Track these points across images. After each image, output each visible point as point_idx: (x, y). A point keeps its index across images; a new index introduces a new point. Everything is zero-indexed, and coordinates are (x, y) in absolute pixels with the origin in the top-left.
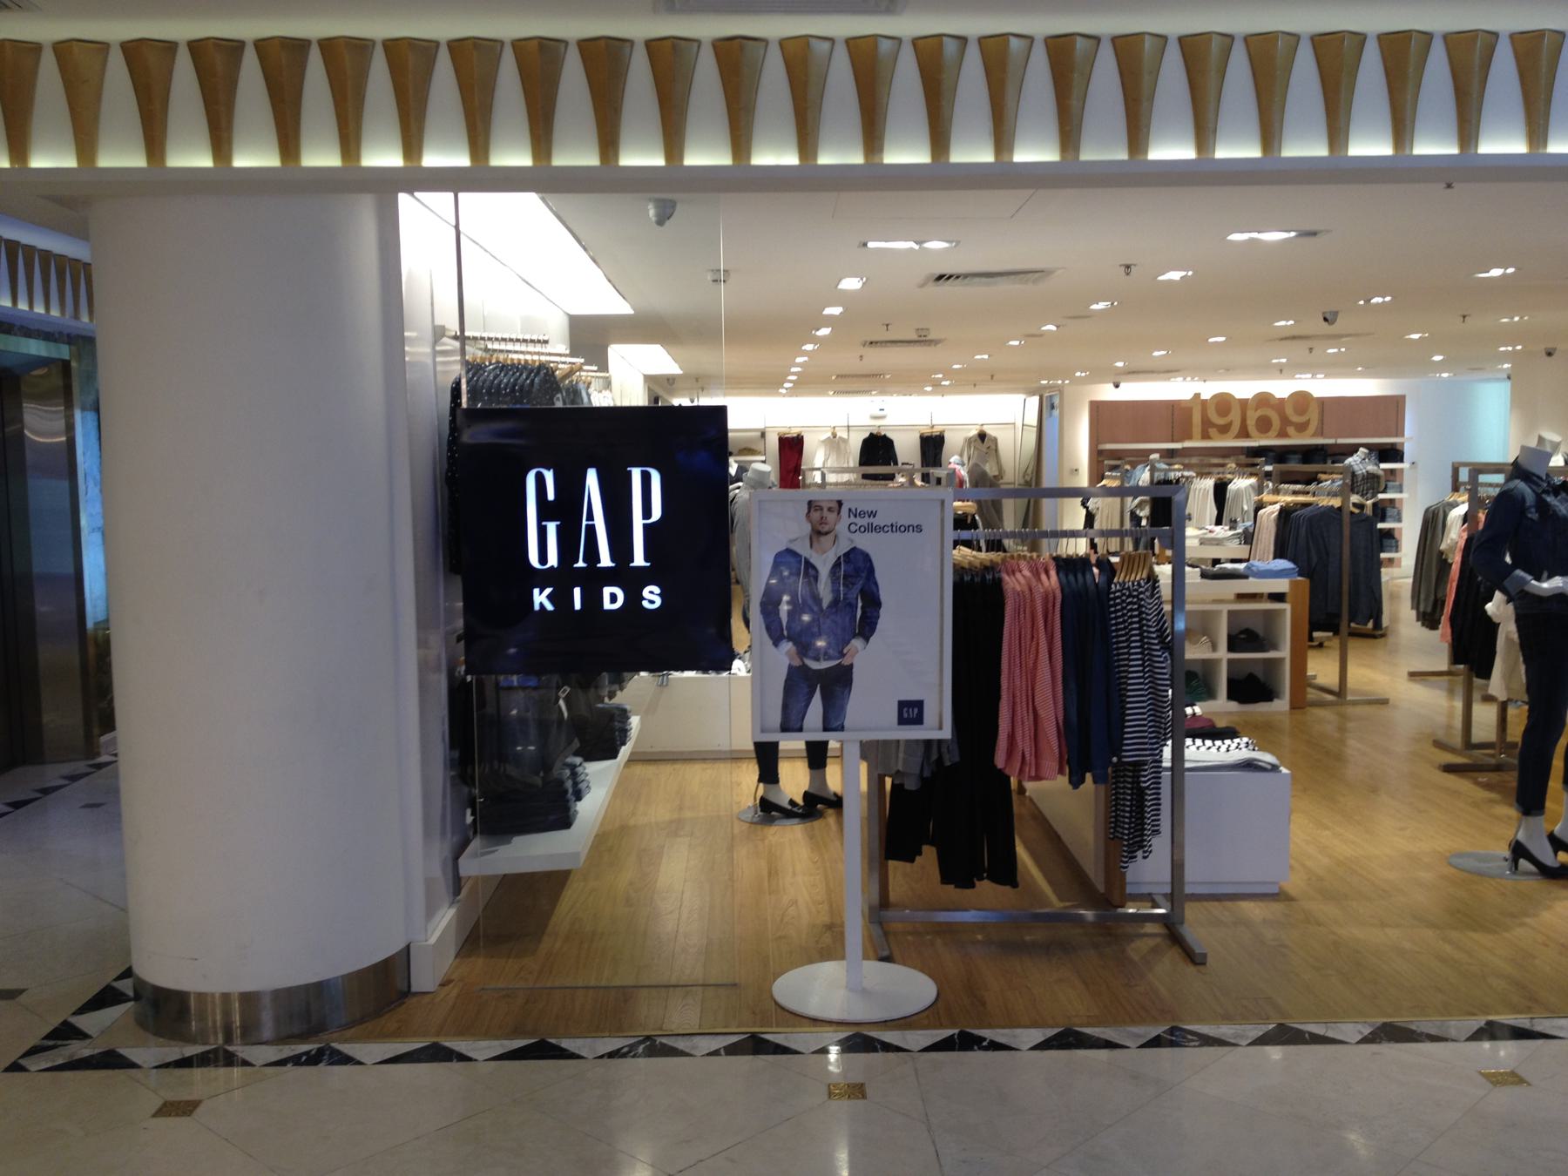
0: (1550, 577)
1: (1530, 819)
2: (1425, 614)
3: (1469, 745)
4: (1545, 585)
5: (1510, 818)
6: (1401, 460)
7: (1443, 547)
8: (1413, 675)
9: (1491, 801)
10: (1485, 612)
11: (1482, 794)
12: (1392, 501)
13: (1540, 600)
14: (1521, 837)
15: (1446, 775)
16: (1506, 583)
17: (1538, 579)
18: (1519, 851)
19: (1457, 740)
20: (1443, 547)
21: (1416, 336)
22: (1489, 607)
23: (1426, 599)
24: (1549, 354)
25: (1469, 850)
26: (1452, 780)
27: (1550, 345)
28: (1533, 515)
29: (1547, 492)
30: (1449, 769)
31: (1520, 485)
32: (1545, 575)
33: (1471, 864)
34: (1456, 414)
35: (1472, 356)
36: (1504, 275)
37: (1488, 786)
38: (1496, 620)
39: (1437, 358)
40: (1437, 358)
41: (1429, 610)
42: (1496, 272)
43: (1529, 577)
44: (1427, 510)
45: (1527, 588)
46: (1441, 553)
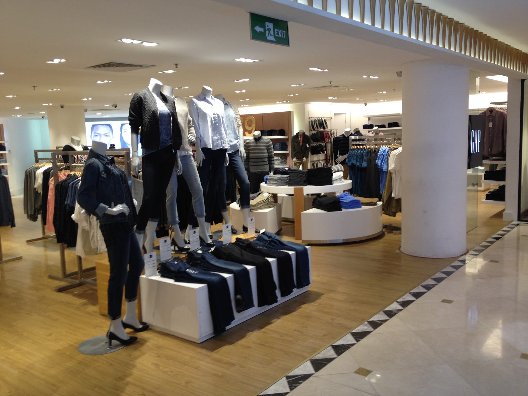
0: (116, 205)
1: (115, 321)
2: (31, 215)
3: (66, 276)
4: (115, 209)
5: (95, 312)
6: (5, 150)
7: (36, 186)
8: (28, 241)
9: (85, 304)
10: (72, 219)
11: (79, 301)
12: (3, 166)
13: (112, 217)
14: (112, 330)
15: (59, 293)
16: (97, 211)
17: (110, 207)
18: (112, 336)
19: (60, 275)
20: (36, 186)
21: (11, 97)
22: (73, 216)
23: (31, 209)
24: (62, 107)
25: (86, 339)
26: (64, 297)
27: (62, 104)
28: (104, 176)
29: (107, 163)
30: (61, 290)
31: (95, 160)
32: (113, 204)
33: (90, 348)
34: (23, 134)
35: (30, 107)
36: (60, 62)
37: (80, 296)
38: (76, 222)
39: (17, 108)
40: (17, 108)
41: (33, 213)
42: (56, 61)
43: (107, 207)
44: (26, 171)
45: (107, 212)
46: (35, 189)
